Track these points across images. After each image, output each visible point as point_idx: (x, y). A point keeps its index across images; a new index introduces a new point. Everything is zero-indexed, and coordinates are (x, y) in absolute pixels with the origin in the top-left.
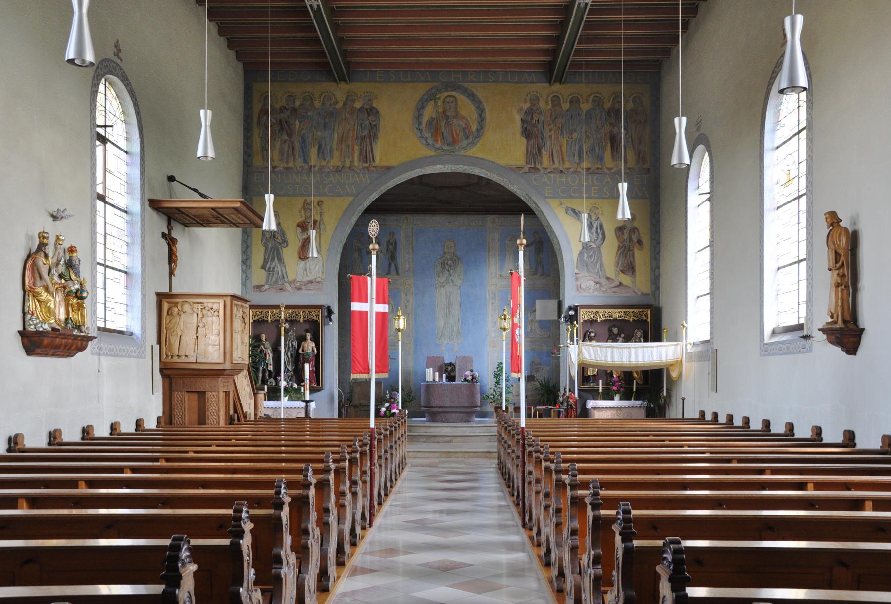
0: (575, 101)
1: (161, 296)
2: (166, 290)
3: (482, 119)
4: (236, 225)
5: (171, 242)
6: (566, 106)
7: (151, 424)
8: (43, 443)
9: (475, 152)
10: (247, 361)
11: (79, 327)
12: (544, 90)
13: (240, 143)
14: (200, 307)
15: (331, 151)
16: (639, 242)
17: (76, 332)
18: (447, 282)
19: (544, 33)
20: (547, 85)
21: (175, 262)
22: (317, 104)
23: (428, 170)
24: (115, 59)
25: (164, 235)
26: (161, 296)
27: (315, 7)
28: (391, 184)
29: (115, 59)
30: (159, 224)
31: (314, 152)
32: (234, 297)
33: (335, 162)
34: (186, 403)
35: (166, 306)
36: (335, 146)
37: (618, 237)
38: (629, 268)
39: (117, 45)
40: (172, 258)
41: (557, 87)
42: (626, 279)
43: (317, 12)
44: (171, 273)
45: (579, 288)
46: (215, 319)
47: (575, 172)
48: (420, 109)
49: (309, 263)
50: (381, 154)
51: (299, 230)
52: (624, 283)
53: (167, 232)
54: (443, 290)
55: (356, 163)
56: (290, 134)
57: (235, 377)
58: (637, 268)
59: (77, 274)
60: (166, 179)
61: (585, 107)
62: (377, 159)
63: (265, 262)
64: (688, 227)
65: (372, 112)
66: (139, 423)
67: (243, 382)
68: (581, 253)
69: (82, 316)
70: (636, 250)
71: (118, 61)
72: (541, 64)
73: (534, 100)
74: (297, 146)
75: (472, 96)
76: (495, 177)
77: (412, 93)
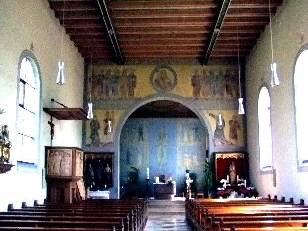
0: (212, 72)
1: (47, 148)
2: (49, 145)
3: (176, 76)
4: (79, 119)
5: (52, 126)
6: (208, 74)
7: (41, 202)
8: (32, 205)
9: (174, 91)
10: (82, 175)
11: (7, 161)
12: (200, 68)
13: (82, 88)
14: (62, 152)
15: (118, 91)
16: (239, 127)
17: (5, 163)
18: (161, 144)
19: (198, 45)
20: (201, 66)
21: (53, 134)
22: (112, 74)
23: (155, 99)
24: (31, 50)
25: (49, 123)
26: (47, 148)
27: (112, 34)
28: (140, 105)
29: (31, 50)
30: (46, 118)
31: (111, 92)
32: (77, 148)
33: (119, 96)
34: (55, 192)
35: (48, 152)
36: (119, 90)
37: (230, 124)
38: (235, 137)
39: (32, 45)
40: (52, 132)
41: (205, 67)
42: (233, 141)
43: (113, 36)
44: (52, 138)
45: (215, 145)
46: (69, 158)
47: (212, 100)
48: (152, 75)
49: (109, 136)
50: (138, 92)
51: (105, 123)
52: (233, 143)
53: (50, 121)
54: (160, 147)
55: (127, 96)
56: (102, 85)
57: (77, 182)
58: (238, 138)
59: (8, 137)
60: (50, 100)
61: (216, 74)
62: (135, 95)
63: (91, 135)
64: (295, 95)
65: (133, 77)
66: (35, 202)
67: (81, 185)
68: (216, 132)
69: (9, 155)
70: (237, 130)
71: (32, 51)
72: (198, 58)
73: (196, 72)
74: (104, 90)
75: (172, 71)
76: (181, 102)
77: (149, 69)
